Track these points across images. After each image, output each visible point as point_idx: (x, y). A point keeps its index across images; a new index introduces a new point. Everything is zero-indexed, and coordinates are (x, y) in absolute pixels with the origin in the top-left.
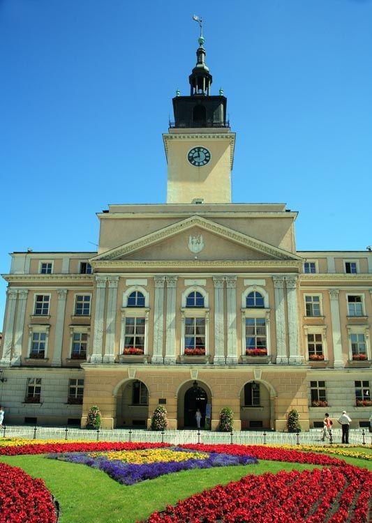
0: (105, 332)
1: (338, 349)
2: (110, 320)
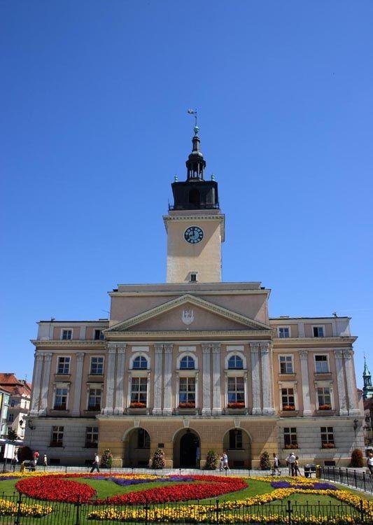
0: (115, 390)
1: (306, 400)
2: (120, 380)
